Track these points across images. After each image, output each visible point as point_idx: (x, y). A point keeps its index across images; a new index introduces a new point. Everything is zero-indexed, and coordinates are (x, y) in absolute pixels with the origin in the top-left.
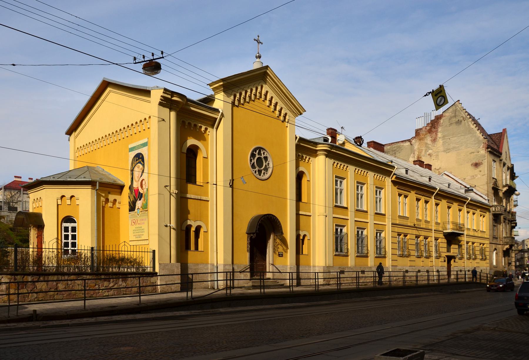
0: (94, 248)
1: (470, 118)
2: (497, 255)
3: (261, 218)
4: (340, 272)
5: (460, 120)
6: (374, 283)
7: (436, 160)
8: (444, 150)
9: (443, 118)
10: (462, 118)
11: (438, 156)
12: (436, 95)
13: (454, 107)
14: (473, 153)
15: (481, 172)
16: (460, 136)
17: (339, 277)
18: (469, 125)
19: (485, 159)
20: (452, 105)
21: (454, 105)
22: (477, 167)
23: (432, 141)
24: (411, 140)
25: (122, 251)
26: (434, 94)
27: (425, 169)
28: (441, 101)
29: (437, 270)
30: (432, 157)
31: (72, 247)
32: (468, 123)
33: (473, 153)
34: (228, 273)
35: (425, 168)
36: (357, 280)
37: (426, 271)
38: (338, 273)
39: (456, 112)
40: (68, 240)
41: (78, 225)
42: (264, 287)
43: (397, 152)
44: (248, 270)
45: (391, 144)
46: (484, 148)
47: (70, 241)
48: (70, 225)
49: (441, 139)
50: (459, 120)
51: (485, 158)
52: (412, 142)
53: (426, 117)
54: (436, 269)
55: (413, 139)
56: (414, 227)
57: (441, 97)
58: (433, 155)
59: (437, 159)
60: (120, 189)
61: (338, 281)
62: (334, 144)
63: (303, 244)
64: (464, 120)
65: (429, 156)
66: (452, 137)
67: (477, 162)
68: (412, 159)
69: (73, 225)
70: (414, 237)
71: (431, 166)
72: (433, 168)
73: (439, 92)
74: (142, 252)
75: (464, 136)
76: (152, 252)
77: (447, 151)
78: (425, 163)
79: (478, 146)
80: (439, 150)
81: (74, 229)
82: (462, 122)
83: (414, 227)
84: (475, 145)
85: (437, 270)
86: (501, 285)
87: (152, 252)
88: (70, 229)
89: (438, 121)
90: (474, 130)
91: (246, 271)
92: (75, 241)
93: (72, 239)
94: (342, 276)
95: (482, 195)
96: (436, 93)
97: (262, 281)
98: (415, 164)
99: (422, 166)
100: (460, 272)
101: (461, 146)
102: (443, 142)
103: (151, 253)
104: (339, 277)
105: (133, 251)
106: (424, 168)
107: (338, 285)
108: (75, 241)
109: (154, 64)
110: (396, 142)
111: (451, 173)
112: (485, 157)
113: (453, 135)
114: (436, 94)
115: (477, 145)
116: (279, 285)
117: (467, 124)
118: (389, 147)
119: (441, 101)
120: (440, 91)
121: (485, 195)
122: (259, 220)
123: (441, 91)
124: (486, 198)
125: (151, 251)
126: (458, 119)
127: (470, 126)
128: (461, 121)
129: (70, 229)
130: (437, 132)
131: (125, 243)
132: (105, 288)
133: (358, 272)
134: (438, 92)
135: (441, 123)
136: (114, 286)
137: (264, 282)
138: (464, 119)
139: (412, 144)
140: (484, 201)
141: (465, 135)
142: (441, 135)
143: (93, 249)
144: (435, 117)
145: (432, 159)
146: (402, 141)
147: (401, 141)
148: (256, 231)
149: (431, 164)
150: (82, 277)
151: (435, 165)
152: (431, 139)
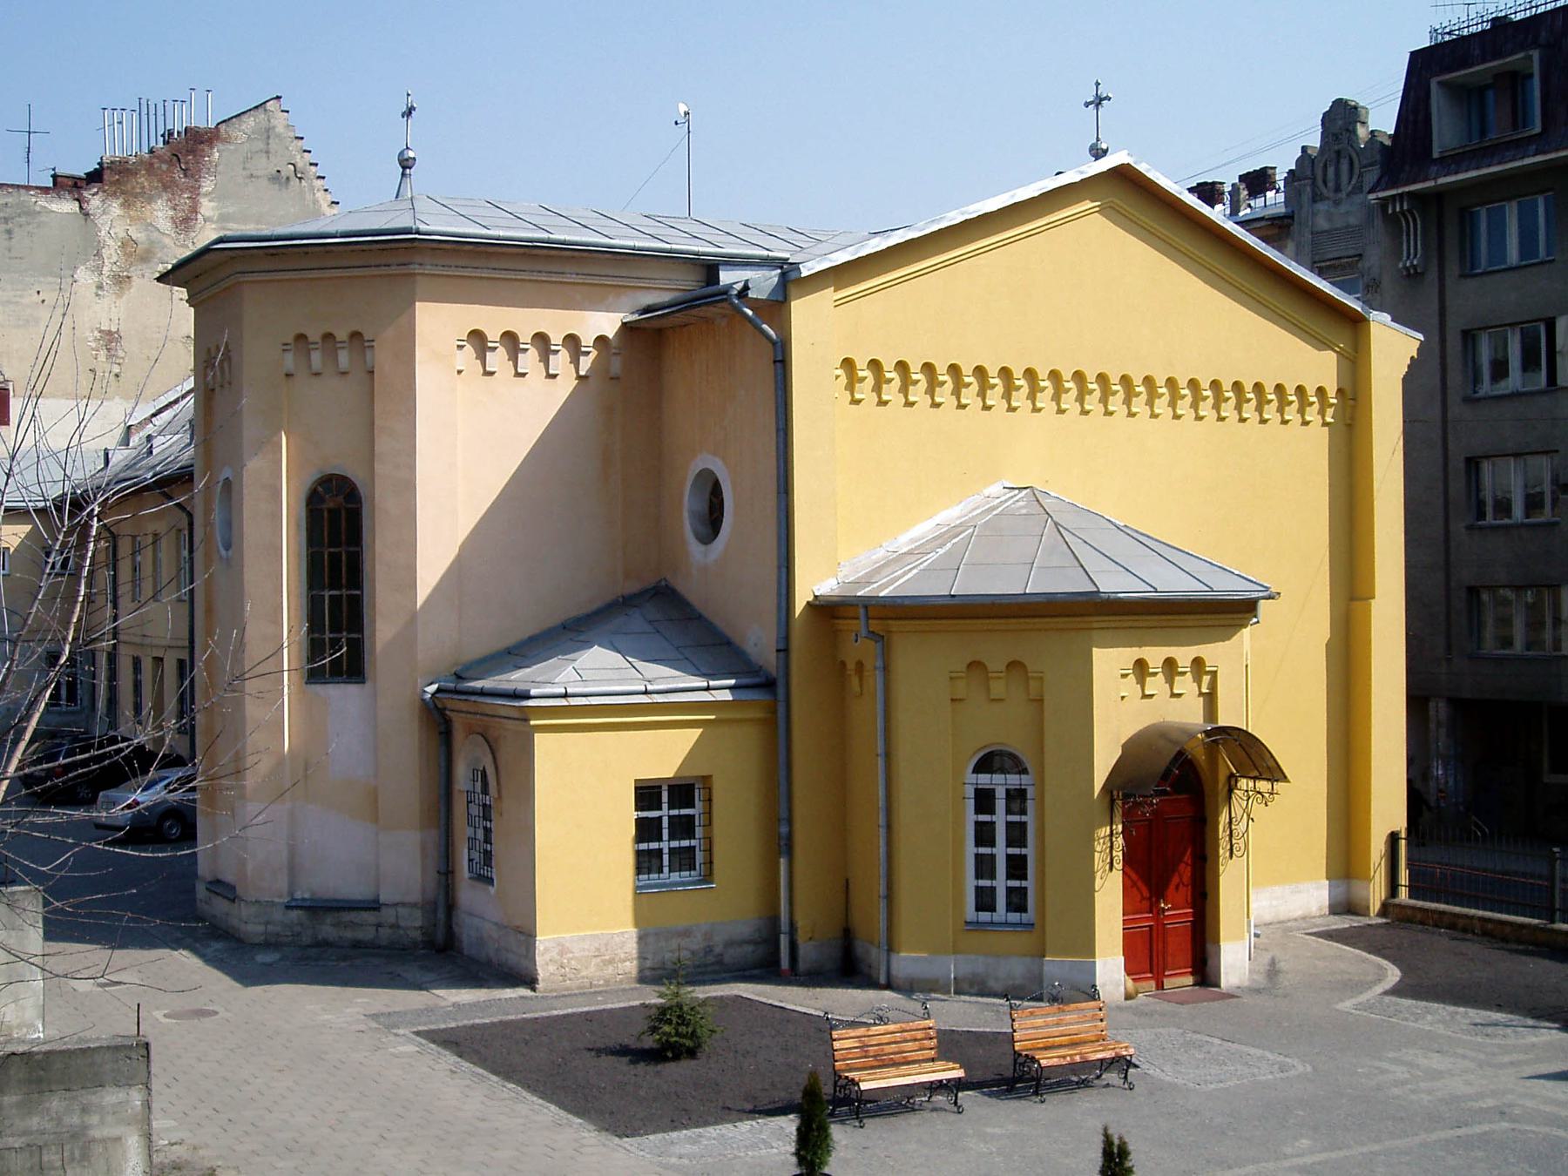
2: (782, 655)
5: (283, 173)
13: (261, 115)
20: (256, 107)
21: (260, 110)
23: (175, 223)
32: (314, 194)
41: (1041, 783)
43: (16, 229)
48: (1000, 783)
49: (213, 226)
50: (278, 171)
52: (88, 202)
64: (300, 178)
65: (7, 236)
69: (1014, 780)
81: (1017, 798)
82: (292, 183)
86: (1557, 846)
109: (1507, 20)
110: (12, 186)
117: (309, 196)
126: (275, 165)
130: (195, 192)
138: (299, 175)
139: (87, 215)
142: (213, 209)
147: (37, 188)
152: (171, 213)
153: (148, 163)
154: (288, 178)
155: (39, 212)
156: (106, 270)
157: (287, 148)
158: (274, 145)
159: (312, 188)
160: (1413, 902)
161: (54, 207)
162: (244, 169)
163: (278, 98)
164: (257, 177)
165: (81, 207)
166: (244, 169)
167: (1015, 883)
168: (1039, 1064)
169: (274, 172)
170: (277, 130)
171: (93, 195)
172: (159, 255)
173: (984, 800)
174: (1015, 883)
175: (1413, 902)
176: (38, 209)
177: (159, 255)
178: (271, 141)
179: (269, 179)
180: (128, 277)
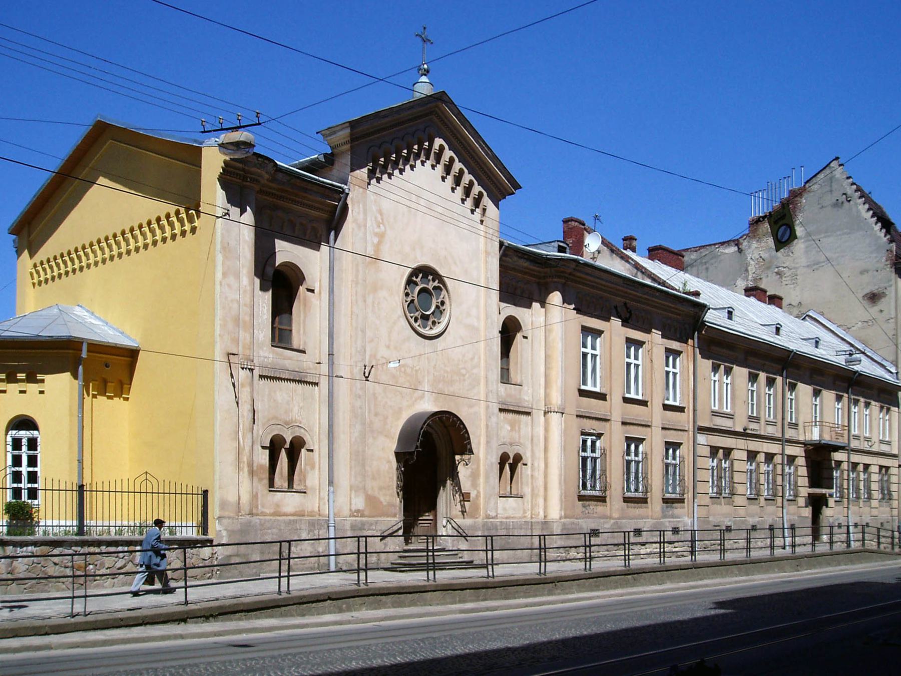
0: (85, 487)
1: (860, 197)
3: (429, 418)
4: (590, 534)
6: (660, 555)
7: (792, 286)
8: (809, 263)
9: (805, 195)
10: (844, 196)
11: (795, 277)
12: (776, 222)
14: (866, 271)
15: (884, 312)
16: (840, 235)
17: (588, 543)
18: (858, 211)
19: (891, 286)
21: (827, 168)
22: (874, 302)
24: (741, 240)
25: (97, 491)
26: (772, 220)
27: (769, 306)
28: (783, 235)
29: (792, 525)
30: (784, 279)
31: (14, 482)
32: (857, 207)
33: (866, 271)
34: (361, 539)
35: (769, 304)
36: (625, 550)
37: (768, 527)
38: (587, 536)
39: (831, 182)
40: (21, 466)
42: (435, 567)
44: (401, 532)
45: (699, 250)
46: (888, 262)
47: (24, 469)
48: (24, 434)
50: (837, 200)
51: (890, 283)
52: (741, 244)
53: (770, 192)
54: (789, 524)
55: (745, 238)
56: (744, 434)
57: (783, 240)
58: (785, 274)
59: (794, 283)
60: (127, 357)
61: (585, 553)
62: (580, 258)
63: (108, 399)
66: (825, 237)
67: (876, 291)
68: (742, 284)
70: (744, 455)
71: (781, 299)
72: (785, 303)
73: (782, 217)
74: (158, 493)
75: (849, 236)
76: (76, 491)
77: (814, 266)
78: (768, 294)
79: (876, 257)
80: (797, 263)
81: (33, 444)
83: (744, 434)
84: (871, 255)
85: (792, 525)
87: (76, 491)
88: (24, 442)
89: (796, 201)
90: (868, 223)
91: (395, 534)
92: (35, 469)
93: (29, 465)
94: (594, 540)
95: (884, 363)
96: (776, 218)
97: (430, 554)
98: (748, 296)
99: (763, 300)
100: (838, 528)
101: (843, 257)
102: (807, 247)
103: (74, 492)
104: (588, 543)
105: (164, 493)
106: (765, 303)
107: (586, 561)
108: (35, 469)
111: (822, 314)
112: (891, 280)
113: (826, 232)
114: (776, 221)
115: (875, 255)
116: (465, 564)
117: (854, 210)
118: (694, 256)
119: (783, 235)
120: (782, 215)
121: (892, 363)
122: (424, 424)
123: (785, 215)
124: (893, 370)
125: (200, 493)
127: (861, 213)
128: (842, 203)
129: (24, 442)
131: (148, 475)
132: (108, 571)
133: (627, 533)
134: (779, 217)
135: (801, 206)
136: (124, 566)
137: (433, 555)
140: (887, 376)
141: (849, 233)
143: (83, 488)
144: (790, 192)
145: (785, 283)
146: (722, 244)
148: (417, 447)
149: (781, 295)
150: (74, 551)
151: (790, 295)
153: (162, 230)
154: (842, 203)
155: (720, 256)
156: (750, 277)
157: (842, 185)
158: (835, 186)
159: (856, 204)
160: (775, 376)
161: (727, 251)
162: (819, 204)
163: (837, 159)
164: (826, 207)
165: (738, 248)
166: (819, 204)
167: (31, 469)
168: (732, 464)
169: (835, 201)
170: (837, 176)
171: (744, 240)
172: (775, 263)
173: (17, 444)
174: (31, 469)
175: (775, 376)
176: (719, 254)
177: (775, 263)
178: (833, 184)
179: (832, 206)
180: (761, 278)
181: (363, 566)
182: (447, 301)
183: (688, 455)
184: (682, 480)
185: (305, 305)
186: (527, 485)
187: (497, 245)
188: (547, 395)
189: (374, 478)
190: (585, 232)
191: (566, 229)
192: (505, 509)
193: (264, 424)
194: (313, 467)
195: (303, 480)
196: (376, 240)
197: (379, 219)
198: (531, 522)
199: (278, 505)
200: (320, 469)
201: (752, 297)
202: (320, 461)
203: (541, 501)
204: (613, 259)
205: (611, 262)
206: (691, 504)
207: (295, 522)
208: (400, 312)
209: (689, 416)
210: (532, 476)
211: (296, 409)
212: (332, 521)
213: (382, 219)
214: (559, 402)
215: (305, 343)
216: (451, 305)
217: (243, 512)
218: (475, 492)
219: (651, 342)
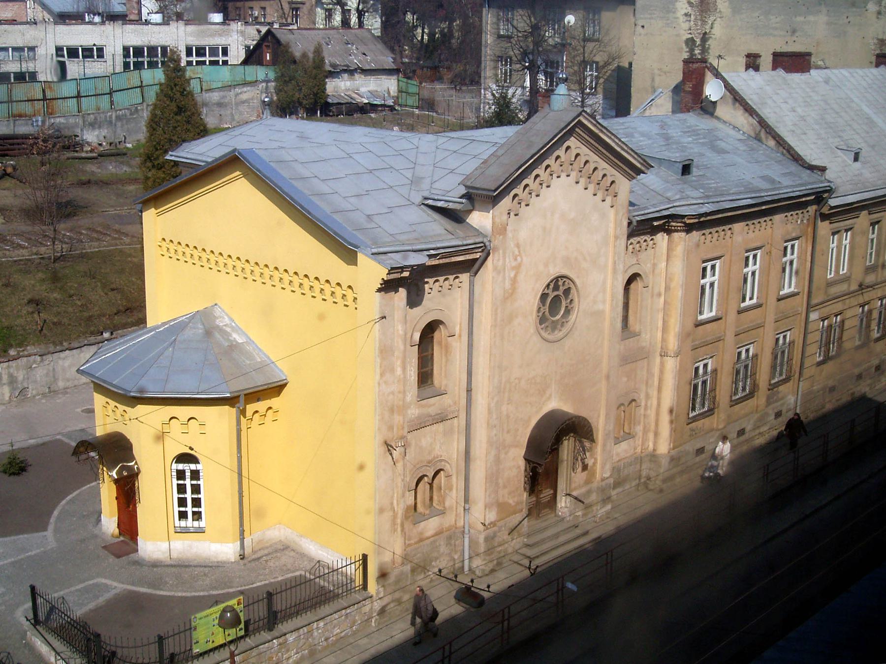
48: (188, 467)
81: (195, 475)
88: (188, 474)
93: (192, 479)
108: (199, 496)
181: (394, 92)
182: (576, 300)
183: (799, 337)
184: (790, 359)
185: (447, 351)
186: (639, 423)
187: (625, 223)
188: (664, 340)
189: (505, 487)
190: (706, 70)
191: (686, 71)
192: (618, 454)
193: (410, 471)
194: (451, 489)
195: (442, 501)
196: (512, 275)
197: (517, 253)
198: (641, 457)
199: (421, 533)
200: (457, 490)
201: (883, 66)
202: (457, 483)
203: (651, 436)
204: (735, 109)
205: (733, 111)
206: (796, 381)
207: (435, 541)
208: (532, 330)
209: (803, 298)
210: (644, 415)
211: (438, 447)
212: (466, 531)
213: (519, 252)
214: (676, 348)
215: (446, 386)
216: (579, 302)
217: (397, 565)
218: (593, 460)
219: (771, 245)
